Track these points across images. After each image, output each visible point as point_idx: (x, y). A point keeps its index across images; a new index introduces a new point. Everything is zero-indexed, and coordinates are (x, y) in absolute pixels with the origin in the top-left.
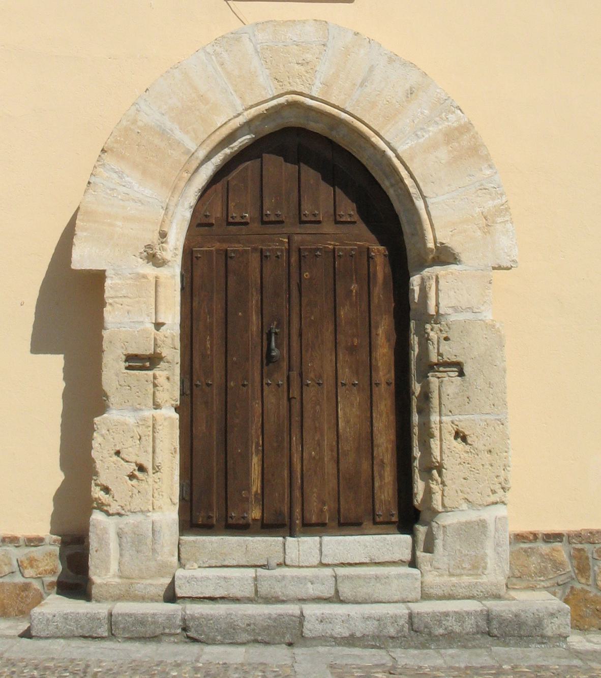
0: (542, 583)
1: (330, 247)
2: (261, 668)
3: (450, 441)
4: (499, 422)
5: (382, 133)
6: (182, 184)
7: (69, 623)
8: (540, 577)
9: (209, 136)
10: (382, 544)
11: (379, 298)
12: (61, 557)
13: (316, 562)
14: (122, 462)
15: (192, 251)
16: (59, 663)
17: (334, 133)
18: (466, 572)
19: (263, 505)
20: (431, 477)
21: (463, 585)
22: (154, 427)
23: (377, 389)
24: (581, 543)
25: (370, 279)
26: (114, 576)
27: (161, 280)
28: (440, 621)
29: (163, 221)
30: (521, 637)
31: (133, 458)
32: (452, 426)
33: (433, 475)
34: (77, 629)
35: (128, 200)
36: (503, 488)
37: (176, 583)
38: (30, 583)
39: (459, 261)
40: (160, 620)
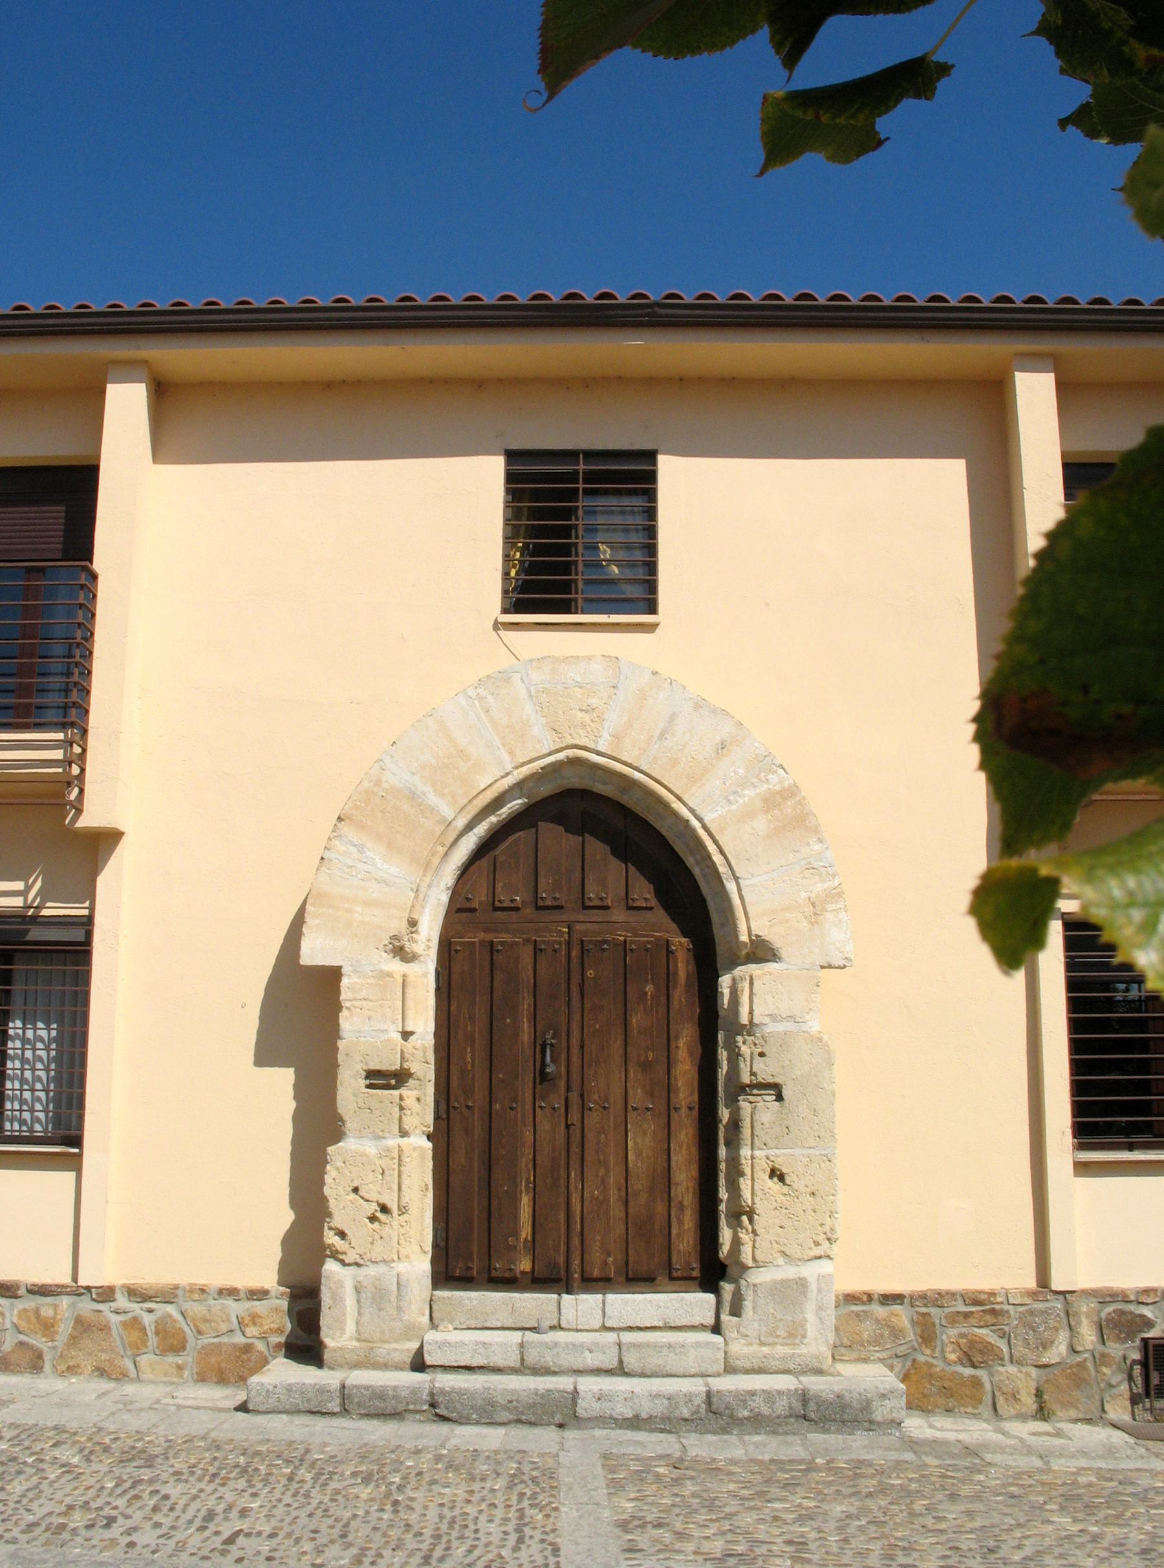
0: (878, 1354)
2: (518, 1457)
3: (763, 1180)
5: (685, 798)
6: (436, 860)
7: (292, 1395)
9: (470, 801)
10: (679, 1305)
12: (290, 1312)
13: (598, 1325)
14: (361, 1200)
15: (450, 943)
16: (274, 1446)
18: (780, 1340)
19: (534, 1256)
20: (740, 1224)
22: (400, 1160)
23: (676, 1115)
24: (926, 1306)
25: (669, 978)
26: (351, 1338)
27: (410, 979)
28: (745, 1401)
30: (843, 1422)
31: (374, 1196)
33: (742, 1221)
36: (829, 1239)
37: (425, 1348)
39: (779, 958)
40: (403, 1393)
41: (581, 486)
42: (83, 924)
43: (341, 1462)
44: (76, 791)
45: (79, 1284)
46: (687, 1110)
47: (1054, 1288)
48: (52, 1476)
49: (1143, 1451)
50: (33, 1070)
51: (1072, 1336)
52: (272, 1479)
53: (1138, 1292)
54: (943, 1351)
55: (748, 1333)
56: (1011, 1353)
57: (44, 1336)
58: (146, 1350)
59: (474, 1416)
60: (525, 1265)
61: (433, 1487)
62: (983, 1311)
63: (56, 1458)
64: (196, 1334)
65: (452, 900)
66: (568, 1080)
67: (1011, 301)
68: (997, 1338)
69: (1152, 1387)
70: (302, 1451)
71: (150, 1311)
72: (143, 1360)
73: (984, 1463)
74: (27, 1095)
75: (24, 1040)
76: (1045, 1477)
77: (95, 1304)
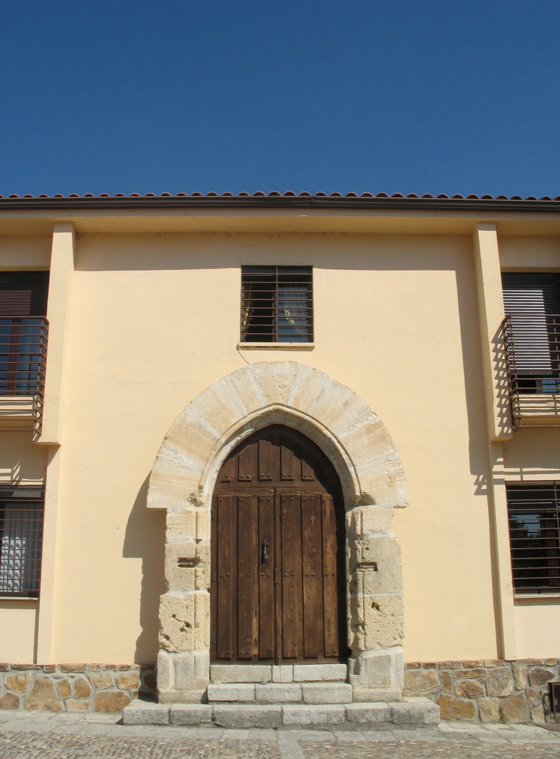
1: (299, 495)
2: (258, 742)
4: (398, 598)
5: (329, 428)
6: (212, 458)
8: (422, 689)
9: (228, 430)
10: (329, 669)
11: (328, 525)
12: (141, 677)
13: (290, 680)
14: (177, 621)
15: (218, 497)
16: (140, 739)
17: (301, 428)
19: (259, 648)
20: (358, 630)
21: (377, 693)
22: (195, 601)
23: (326, 578)
24: (446, 669)
25: (322, 514)
26: (172, 688)
27: (200, 514)
28: (363, 715)
29: (201, 479)
30: (411, 724)
31: (183, 619)
32: (370, 600)
33: (359, 629)
34: (150, 719)
35: (180, 467)
36: (400, 637)
37: (208, 692)
38: (122, 693)
39: (375, 503)
41: (277, 282)
42: (40, 489)
43: (174, 745)
44: (38, 425)
45: (38, 664)
46: (332, 576)
47: (506, 659)
48: (35, 754)
49: (553, 736)
50: (14, 560)
51: (515, 682)
52: (143, 753)
53: (546, 661)
54: (454, 691)
55: (363, 682)
56: (487, 691)
57: (20, 690)
58: (70, 696)
59: (233, 725)
60: (255, 651)
61: (221, 755)
62: (473, 671)
63: (35, 746)
64: (95, 688)
65: (219, 476)
66: (275, 562)
67: (476, 198)
68: (480, 684)
69: (554, 706)
70: (154, 741)
71: (72, 677)
72: (69, 701)
73: (479, 742)
74: (11, 572)
75: (9, 546)
76: (510, 747)
77: (45, 674)
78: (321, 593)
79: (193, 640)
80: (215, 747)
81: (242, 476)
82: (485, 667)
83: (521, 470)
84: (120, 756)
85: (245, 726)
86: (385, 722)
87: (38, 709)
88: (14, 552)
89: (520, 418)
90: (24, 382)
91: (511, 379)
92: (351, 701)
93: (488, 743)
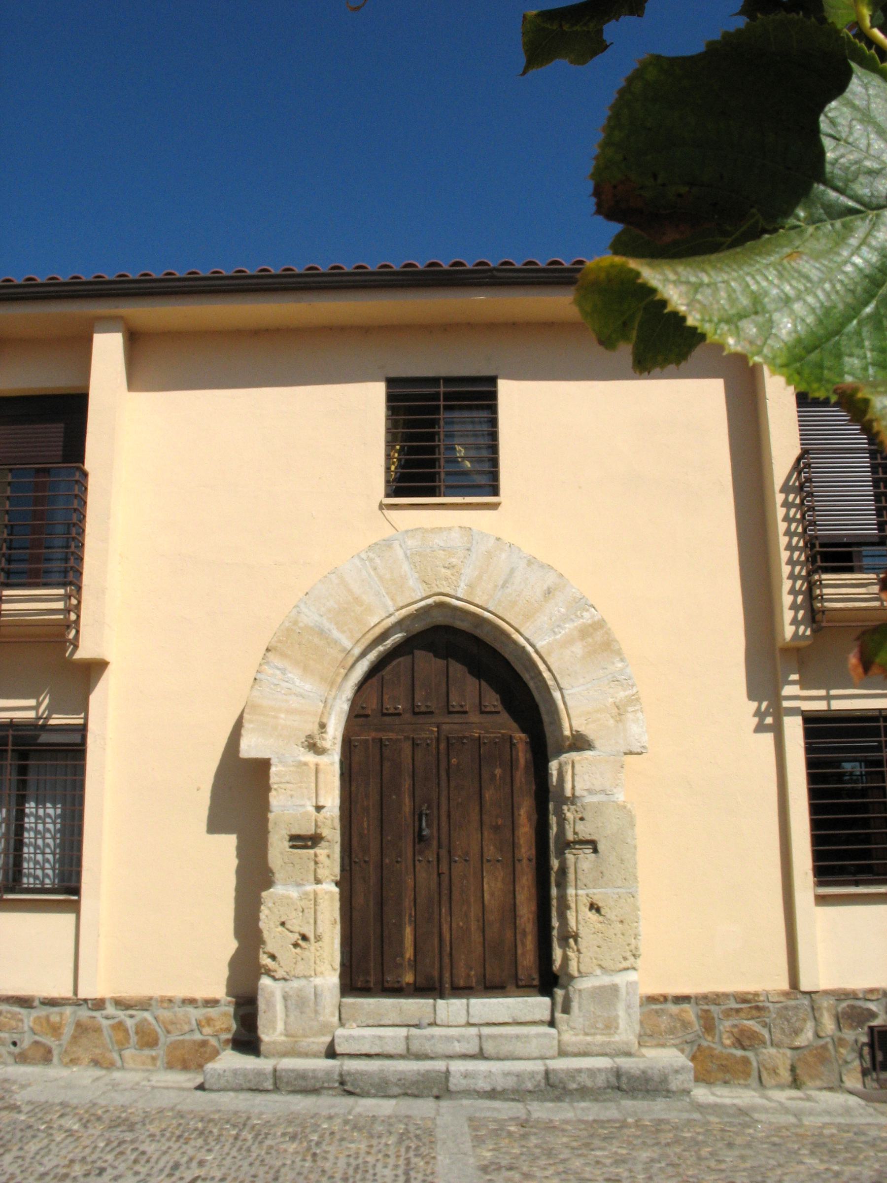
5: (522, 630)
6: (339, 679)
8: (669, 1035)
13: (463, 1021)
25: (512, 764)
26: (281, 1034)
27: (321, 767)
28: (574, 1077)
29: (323, 713)
31: (296, 929)
36: (634, 955)
39: (593, 747)
41: (442, 403)
43: (274, 1125)
44: (73, 632)
48: (58, 1139)
50: (44, 838)
54: (721, 1038)
57: (53, 1036)
60: (409, 978)
62: (750, 1008)
71: (132, 1016)
72: (127, 1053)
75: (37, 817)
78: (512, 888)
79: (312, 961)
80: (336, 1128)
81: (388, 707)
82: (769, 1002)
83: (828, 693)
84: (186, 1143)
85: (391, 1094)
86: (608, 1087)
87: (80, 1064)
88: (44, 826)
89: (823, 611)
90: (57, 565)
91: (811, 550)
92: (556, 1055)
93: (765, 1123)
